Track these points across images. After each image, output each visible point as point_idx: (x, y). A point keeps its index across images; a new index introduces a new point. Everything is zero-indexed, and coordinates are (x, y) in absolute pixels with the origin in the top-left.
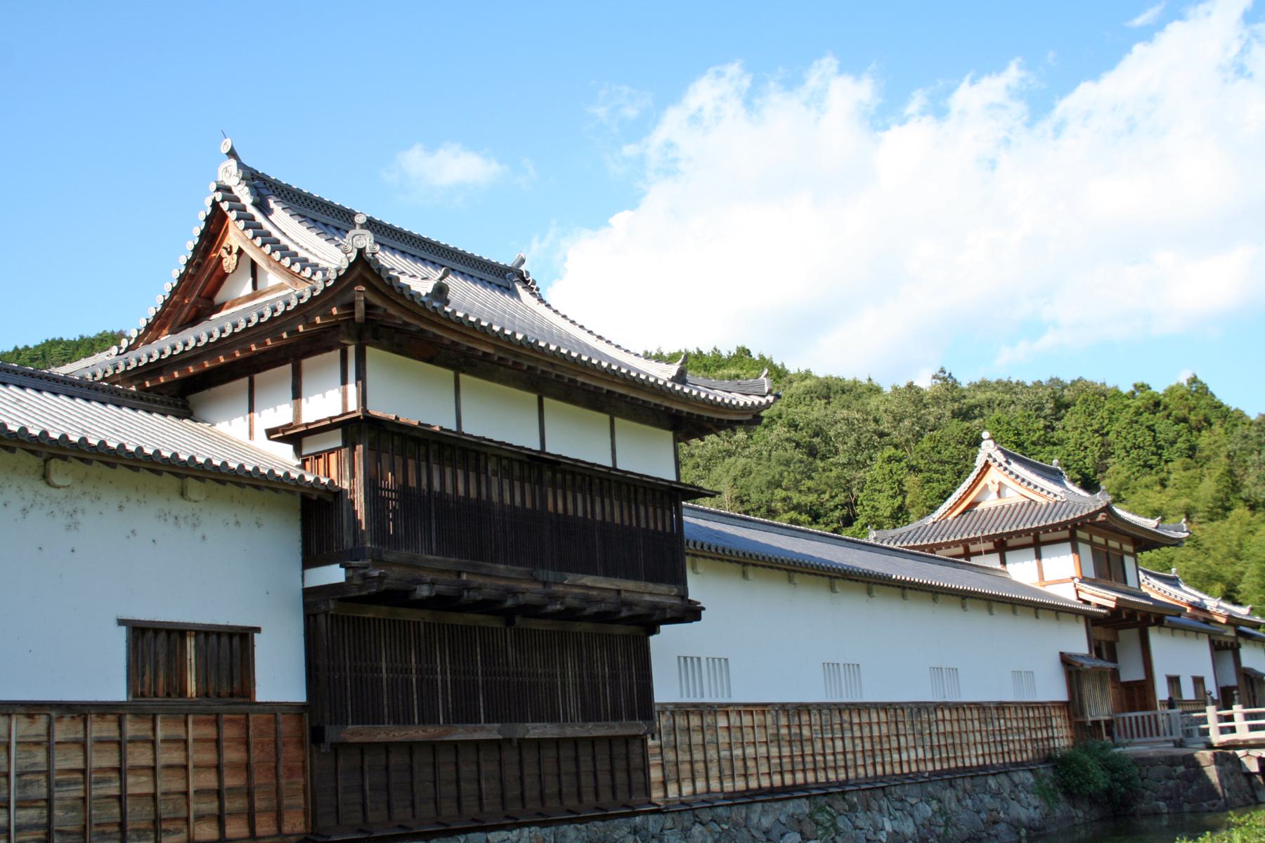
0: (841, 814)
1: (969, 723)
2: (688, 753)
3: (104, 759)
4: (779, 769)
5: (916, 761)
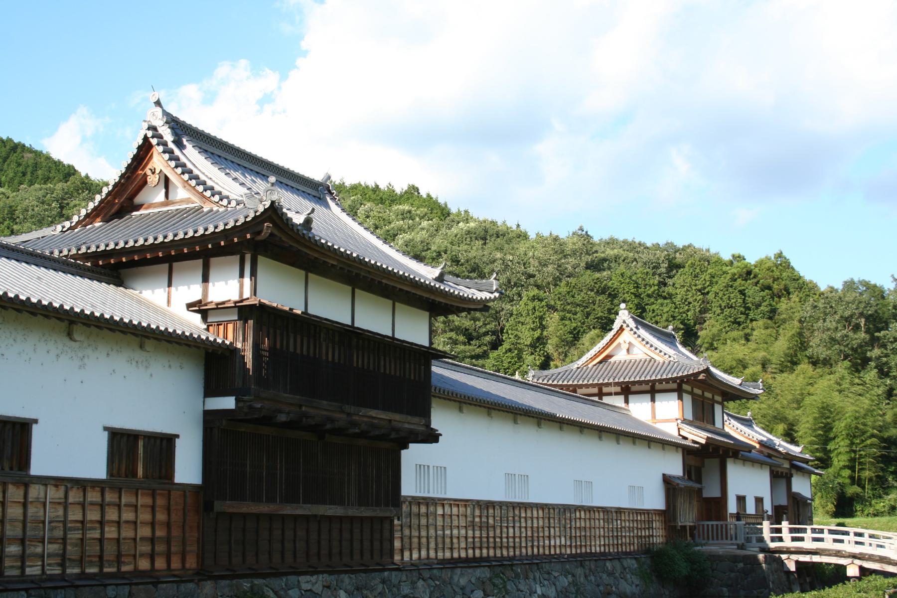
0: (509, 580)
1: (597, 521)
2: (418, 531)
3: (93, 515)
4: (472, 546)
5: (560, 546)
